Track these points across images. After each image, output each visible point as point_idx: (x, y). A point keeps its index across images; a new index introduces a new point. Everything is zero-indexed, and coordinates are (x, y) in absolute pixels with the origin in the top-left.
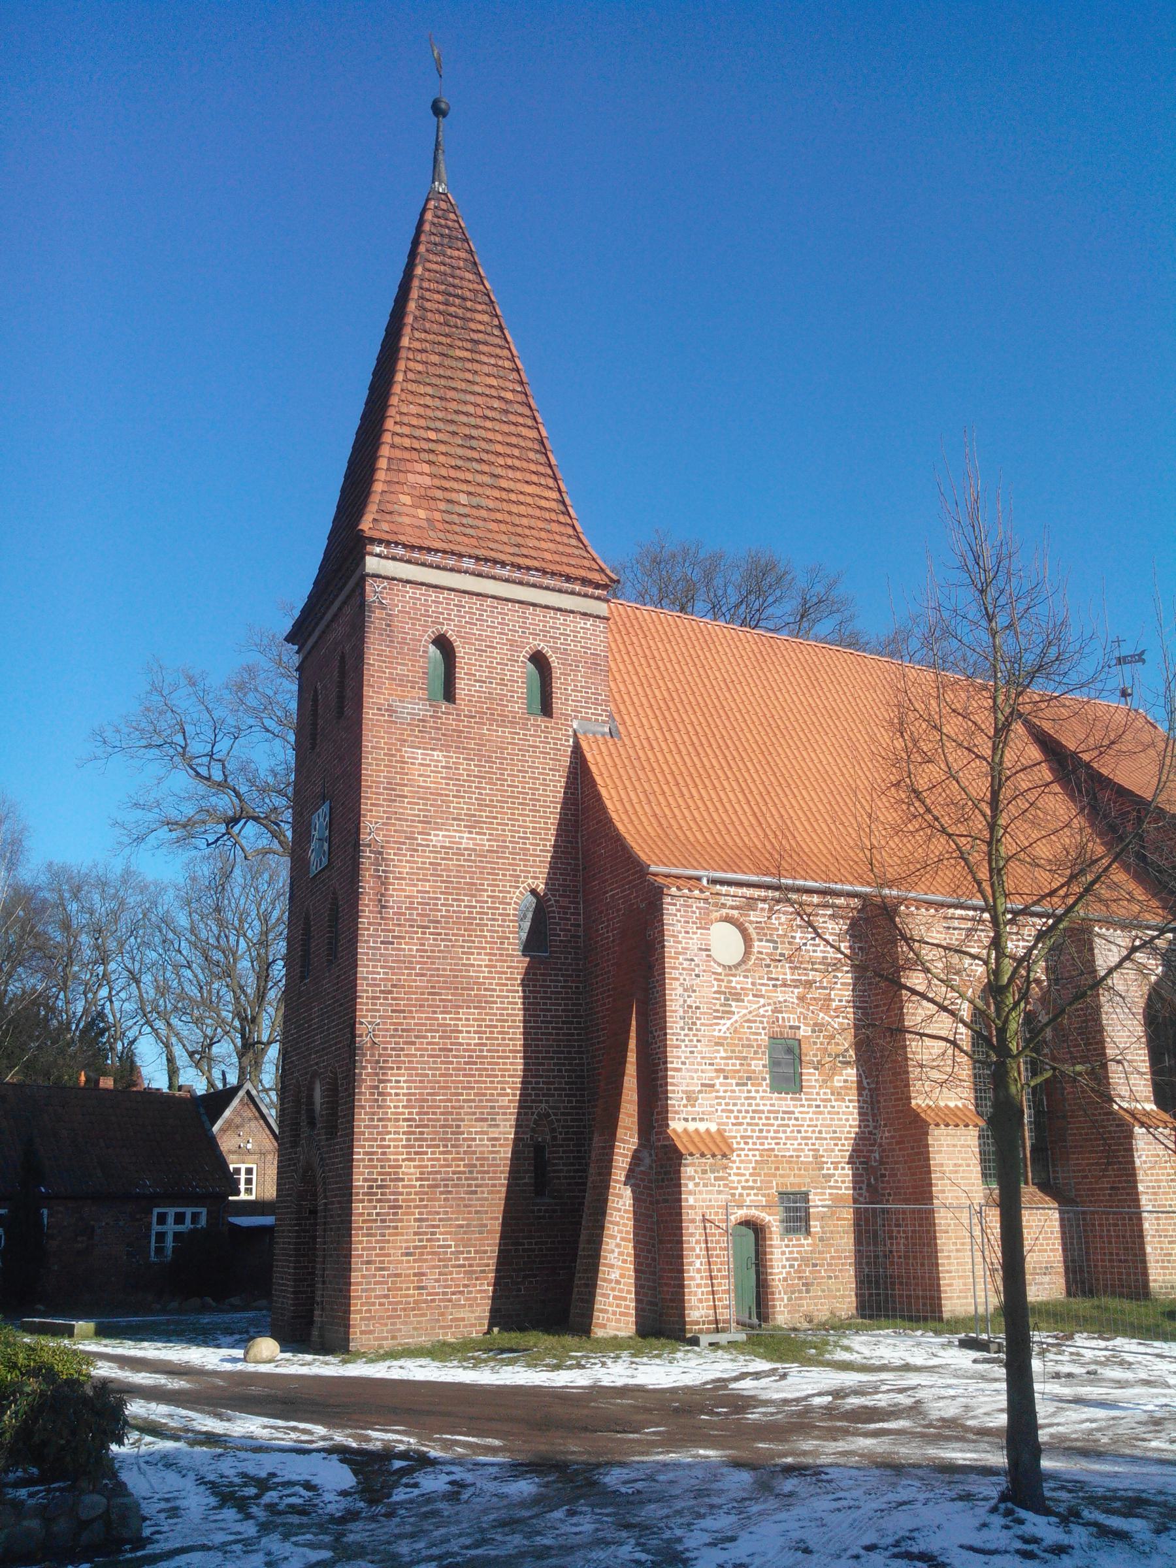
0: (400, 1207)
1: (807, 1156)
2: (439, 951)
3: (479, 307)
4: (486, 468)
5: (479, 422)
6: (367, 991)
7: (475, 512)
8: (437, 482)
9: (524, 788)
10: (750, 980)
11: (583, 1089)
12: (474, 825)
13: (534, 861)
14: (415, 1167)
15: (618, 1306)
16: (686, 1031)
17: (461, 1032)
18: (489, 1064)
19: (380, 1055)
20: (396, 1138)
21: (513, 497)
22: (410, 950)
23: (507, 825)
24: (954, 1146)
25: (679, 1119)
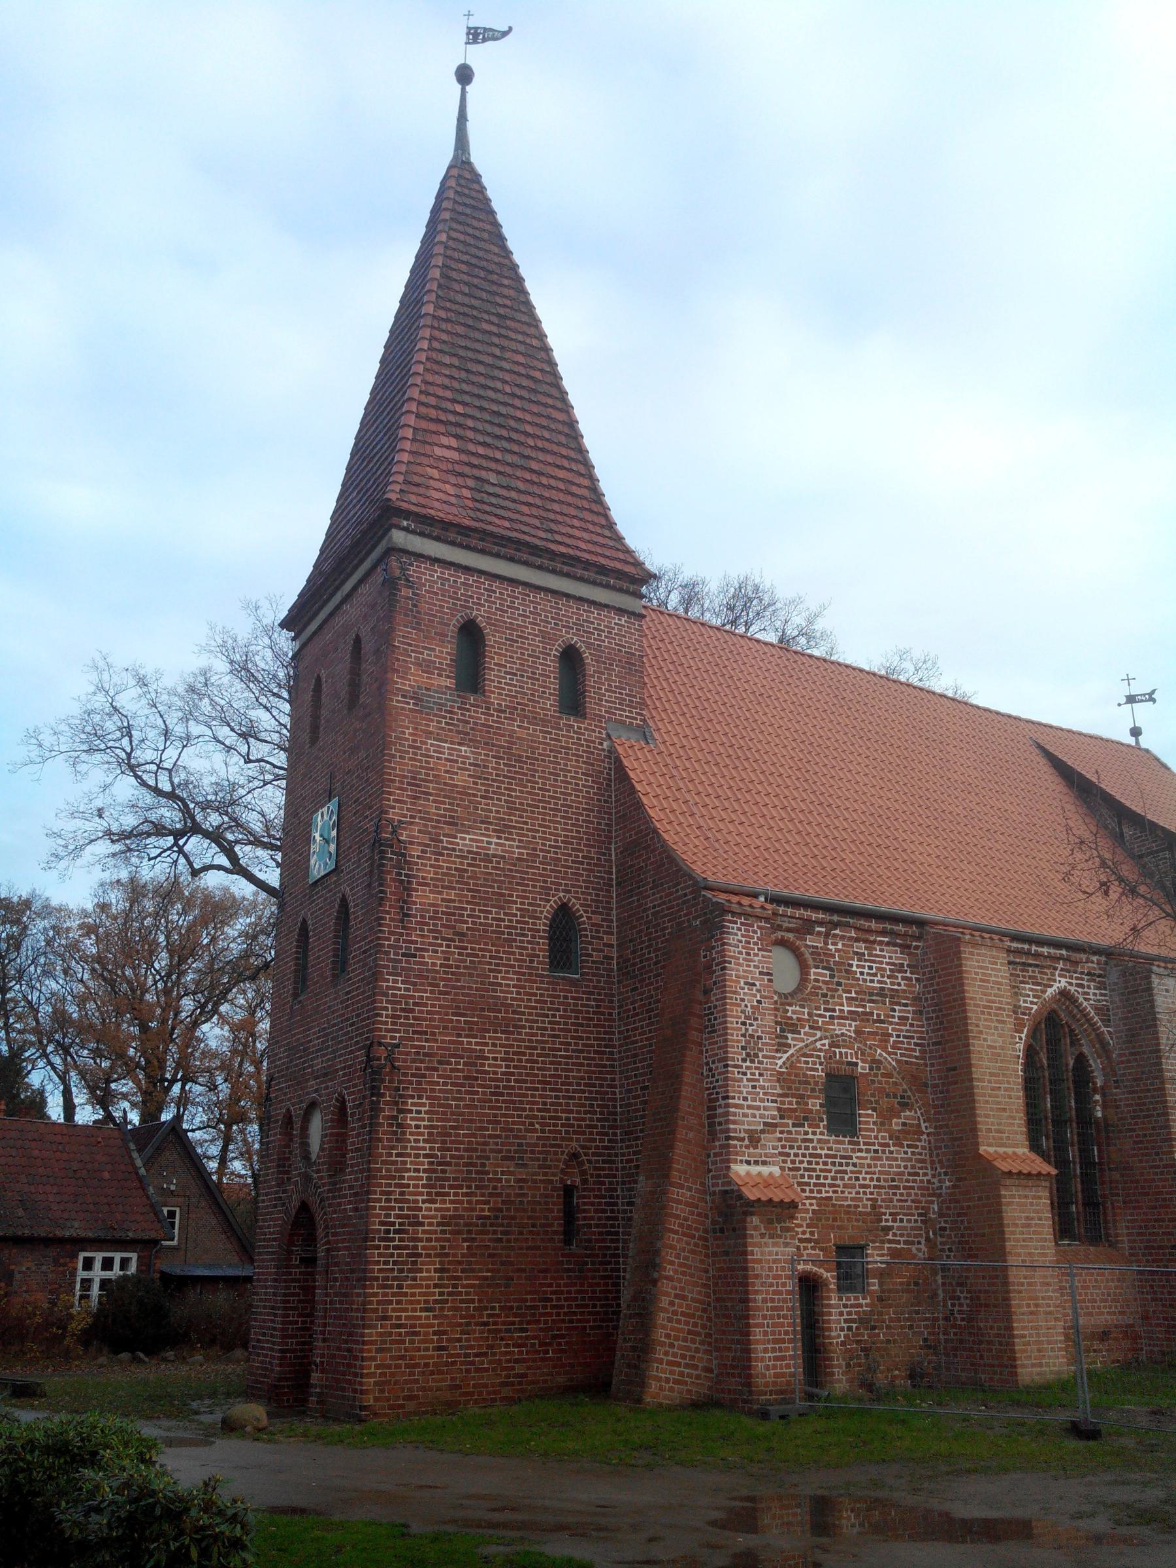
0: (420, 1255)
2: (465, 967)
3: (506, 282)
4: (516, 448)
5: (507, 399)
6: (386, 1009)
7: (504, 492)
8: (464, 458)
9: (556, 792)
10: (806, 1010)
11: (616, 1127)
12: (503, 830)
13: (566, 873)
14: (436, 1209)
15: (672, 1372)
16: (748, 1064)
17: (487, 1058)
18: (517, 1095)
19: (400, 1082)
20: (415, 1174)
21: (544, 481)
22: (434, 964)
23: (538, 831)
24: (1026, 1197)
25: (741, 1161)
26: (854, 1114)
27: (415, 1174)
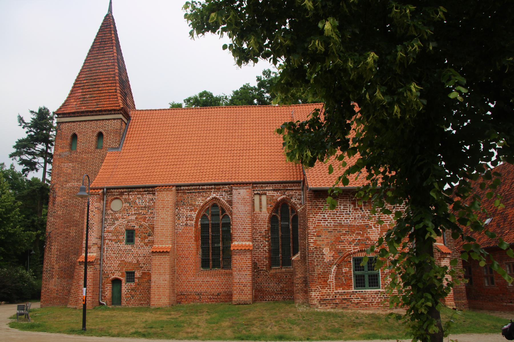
1: (135, 261)
20: (54, 259)
27: (54, 259)
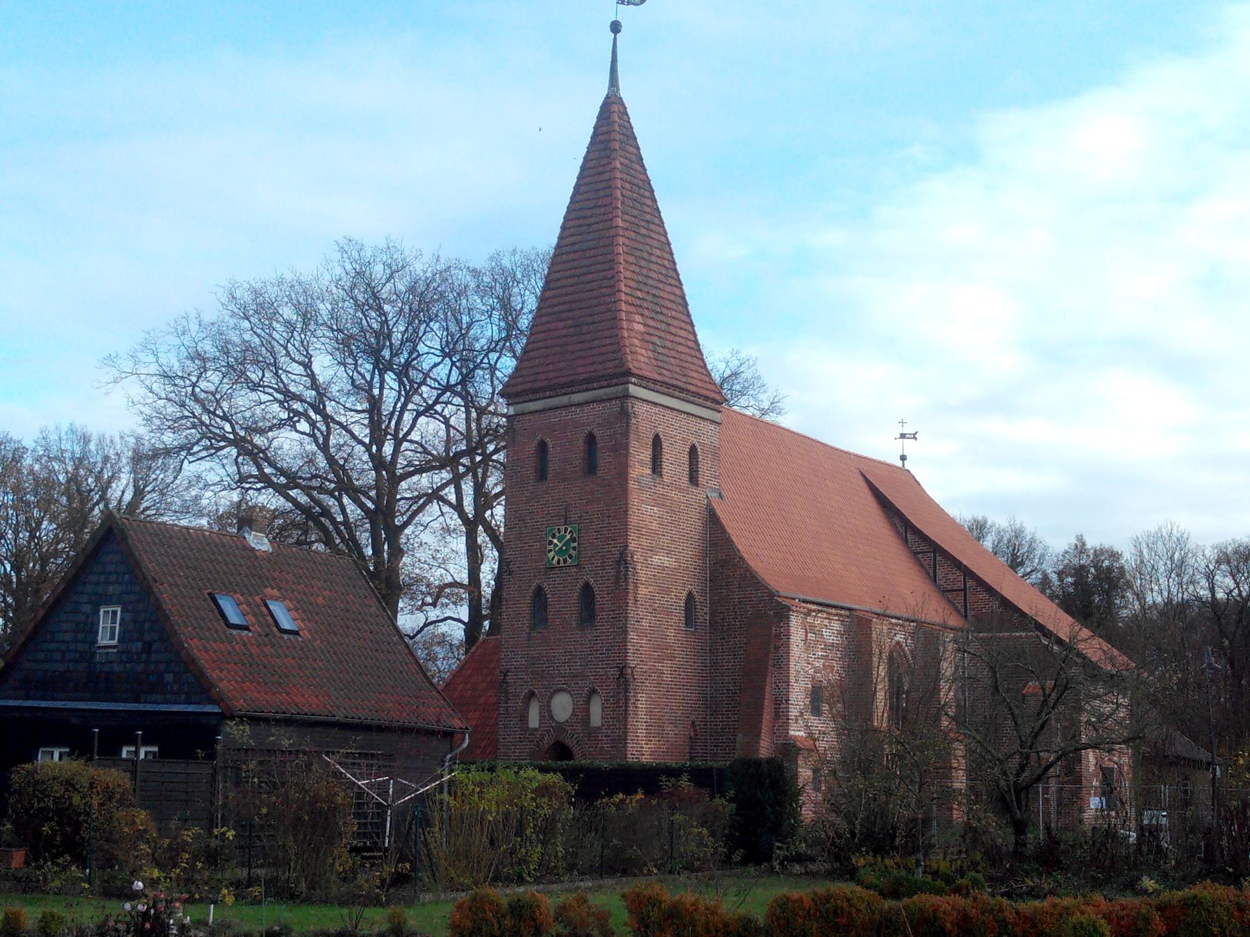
20: (642, 733)
26: (819, 707)
27: (642, 733)
